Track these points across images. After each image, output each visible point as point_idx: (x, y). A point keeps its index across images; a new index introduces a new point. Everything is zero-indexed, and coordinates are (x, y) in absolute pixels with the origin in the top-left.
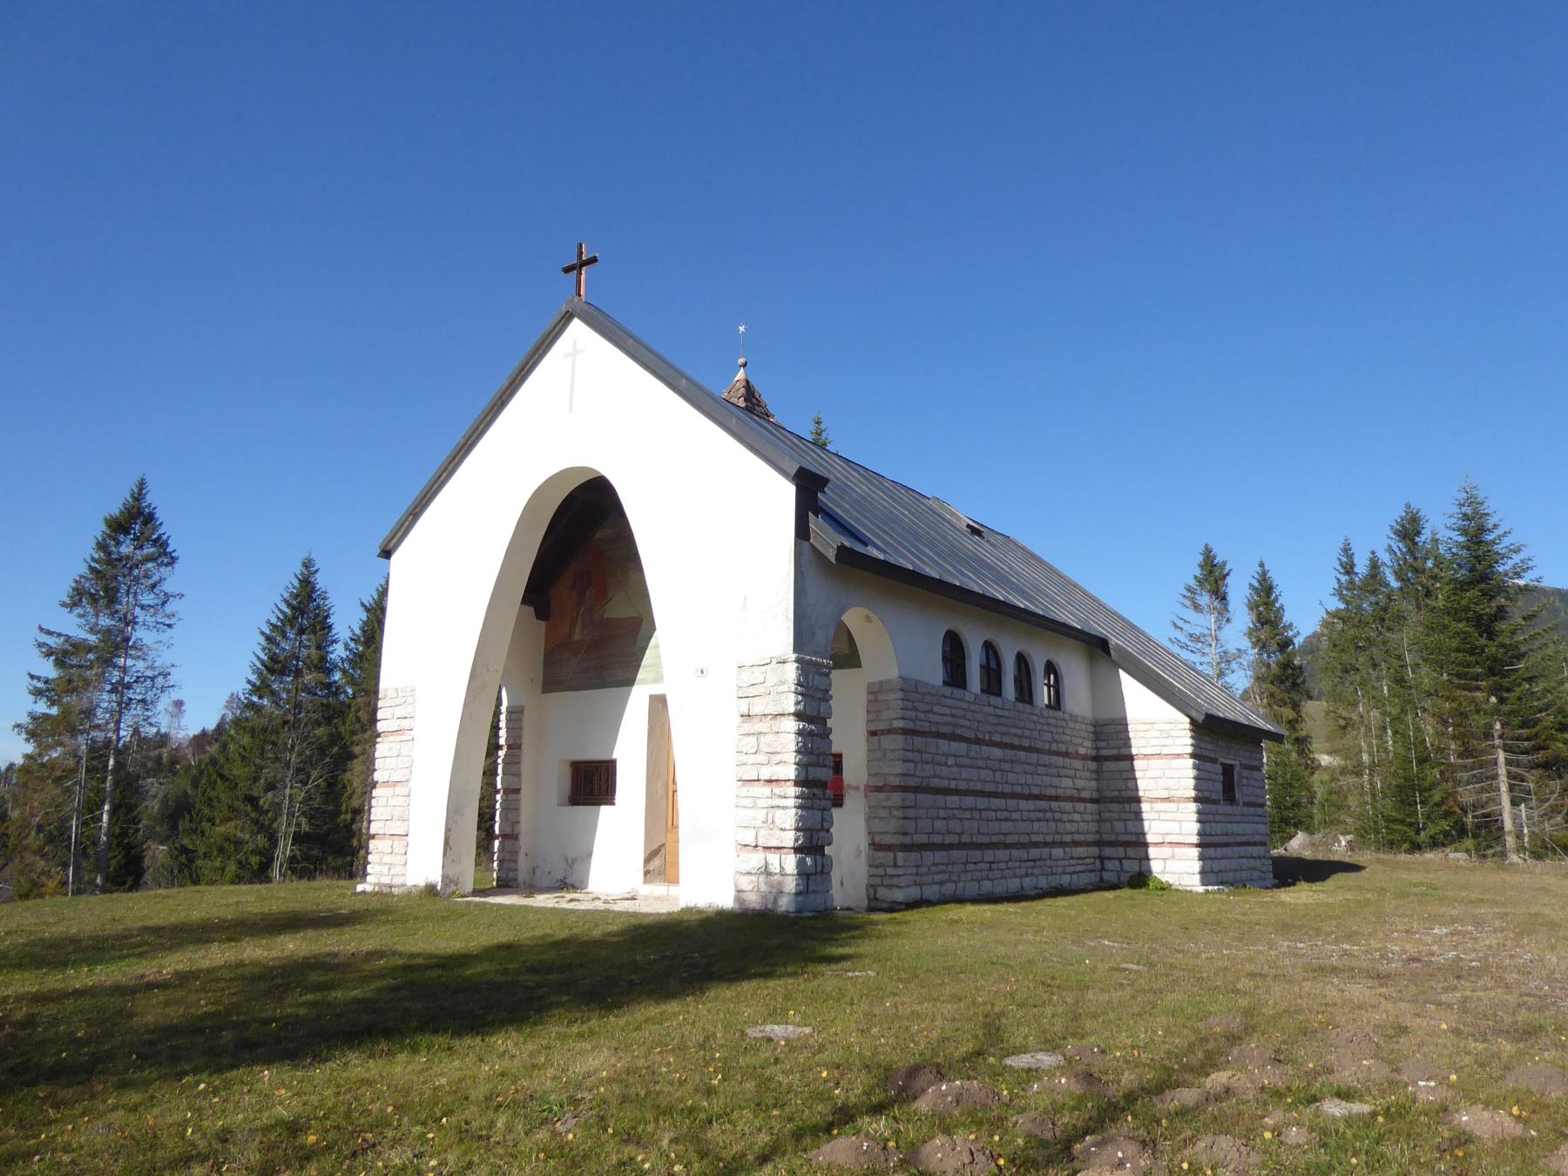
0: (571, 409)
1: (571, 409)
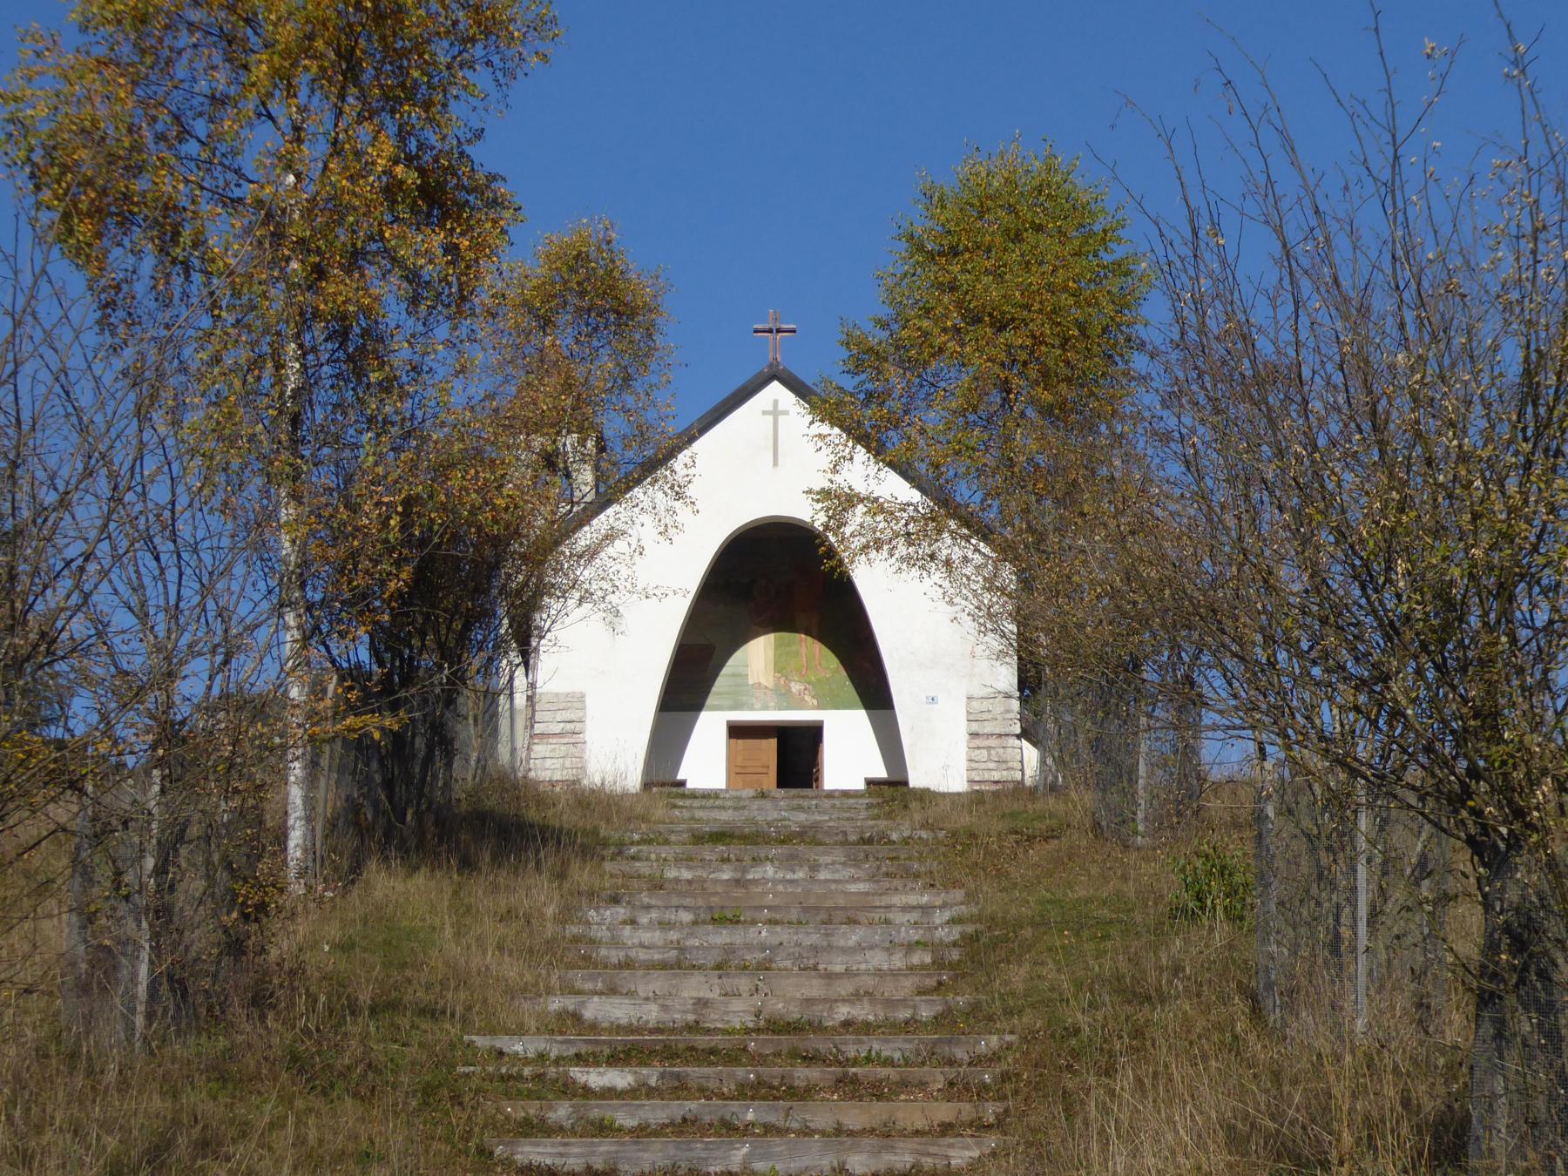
0: (775, 463)
1: (775, 463)
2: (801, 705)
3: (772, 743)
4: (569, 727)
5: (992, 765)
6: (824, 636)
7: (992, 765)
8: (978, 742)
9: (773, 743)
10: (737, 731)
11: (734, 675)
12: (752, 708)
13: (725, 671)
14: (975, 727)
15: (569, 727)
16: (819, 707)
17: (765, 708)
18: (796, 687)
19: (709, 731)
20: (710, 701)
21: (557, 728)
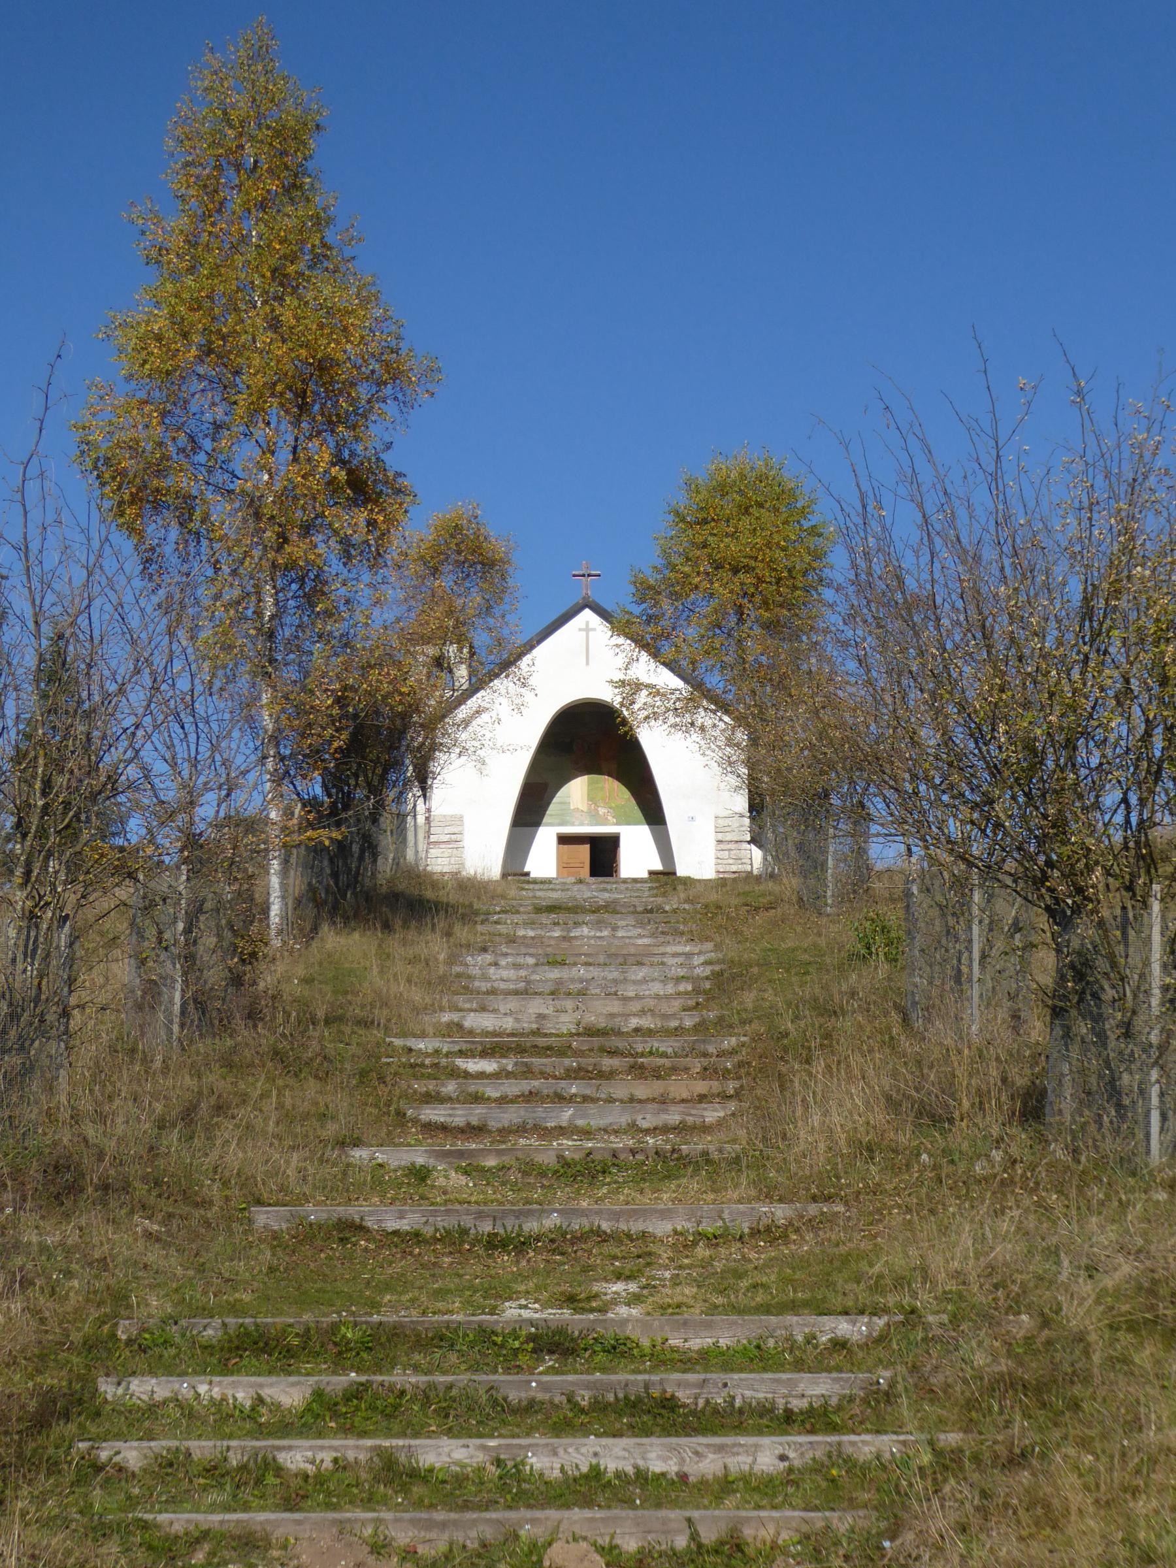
0: (587, 663)
1: (587, 663)
2: (605, 822)
3: (586, 849)
4: (454, 837)
5: (731, 861)
6: (620, 777)
7: (731, 861)
8: (722, 846)
9: (587, 847)
10: (563, 840)
11: (561, 803)
12: (573, 825)
13: (555, 800)
14: (720, 836)
15: (454, 837)
16: (617, 824)
17: (582, 824)
18: (602, 811)
19: (545, 841)
20: (545, 820)
21: (446, 838)
